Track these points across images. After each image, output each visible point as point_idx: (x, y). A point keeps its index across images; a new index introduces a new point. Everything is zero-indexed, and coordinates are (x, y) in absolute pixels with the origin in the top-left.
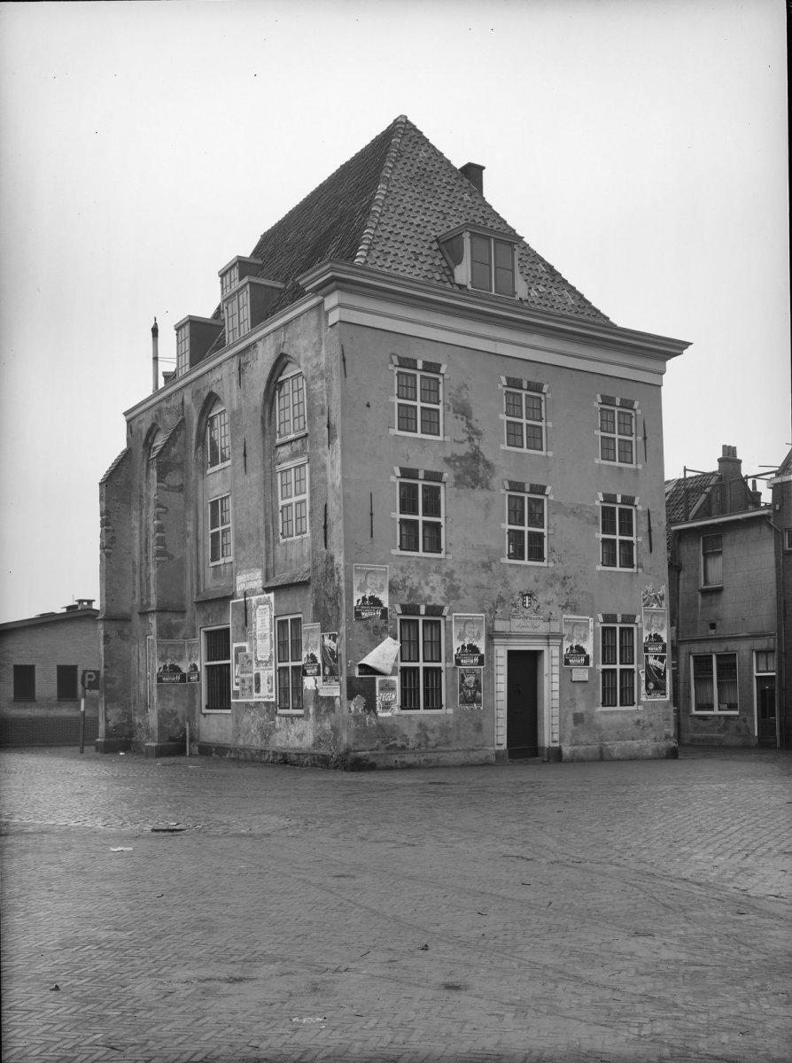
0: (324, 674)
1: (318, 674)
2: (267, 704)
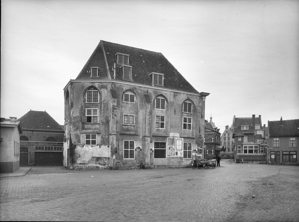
0: (198, 153)
1: (196, 153)
2: (180, 158)
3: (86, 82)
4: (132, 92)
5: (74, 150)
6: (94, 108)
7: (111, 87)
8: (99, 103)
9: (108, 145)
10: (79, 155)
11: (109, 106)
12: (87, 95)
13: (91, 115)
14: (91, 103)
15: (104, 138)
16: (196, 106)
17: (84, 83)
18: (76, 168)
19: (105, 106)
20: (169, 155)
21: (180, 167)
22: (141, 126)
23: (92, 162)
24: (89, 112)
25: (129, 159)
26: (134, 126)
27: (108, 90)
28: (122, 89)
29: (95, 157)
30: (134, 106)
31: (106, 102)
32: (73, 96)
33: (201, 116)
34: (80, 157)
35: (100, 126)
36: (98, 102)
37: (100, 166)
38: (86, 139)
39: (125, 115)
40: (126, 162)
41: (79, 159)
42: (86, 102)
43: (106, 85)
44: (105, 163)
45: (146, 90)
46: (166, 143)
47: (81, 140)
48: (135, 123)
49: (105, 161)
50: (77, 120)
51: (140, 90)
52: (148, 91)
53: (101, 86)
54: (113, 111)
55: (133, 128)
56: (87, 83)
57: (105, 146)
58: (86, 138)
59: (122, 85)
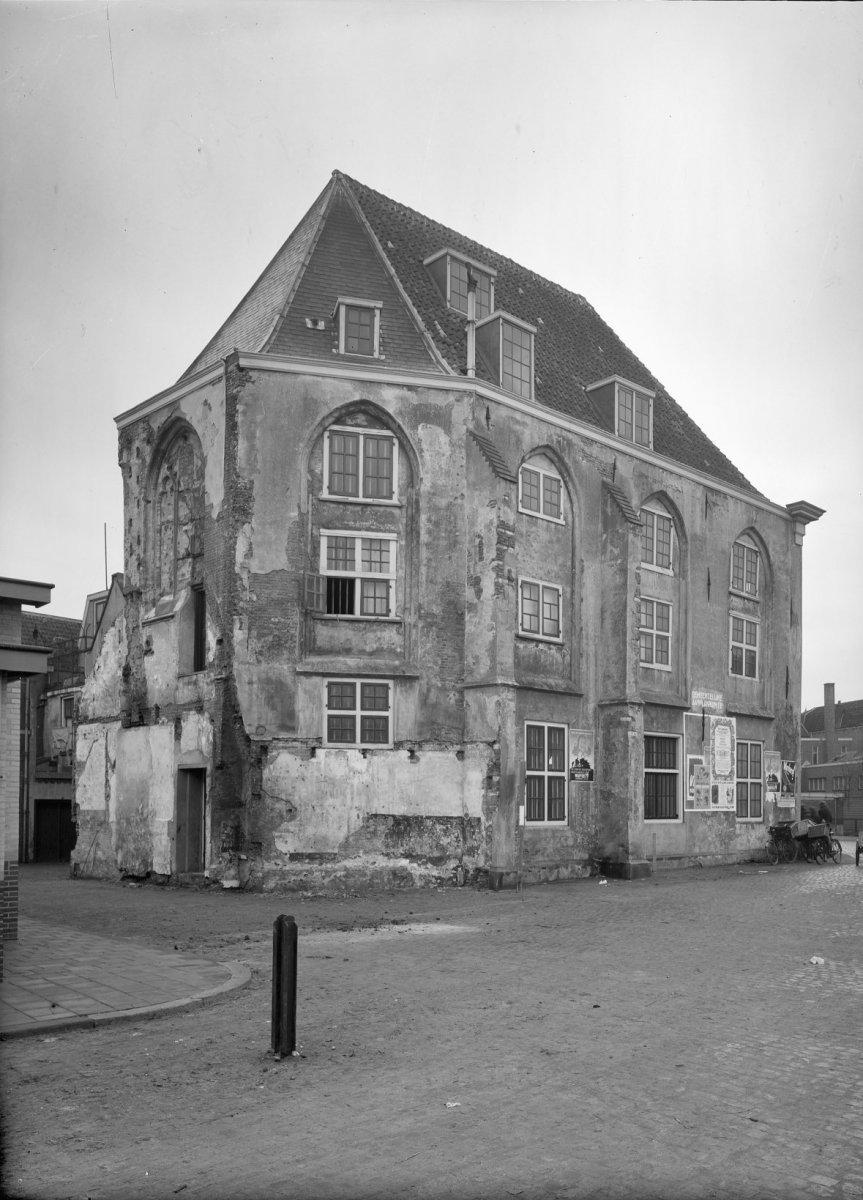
1: (778, 791)
2: (726, 813)
3: (330, 377)
4: (552, 461)
5: (249, 775)
6: (368, 529)
7: (474, 418)
8: (400, 507)
9: (458, 748)
10: (288, 802)
11: (459, 522)
12: (332, 453)
13: (353, 569)
14: (351, 499)
15: (435, 706)
16: (775, 567)
17: (317, 383)
18: (271, 884)
19: (437, 524)
20: (691, 804)
21: (730, 861)
22: (591, 649)
23: (368, 845)
24: (342, 551)
25: (546, 823)
26: (560, 646)
27: (455, 437)
28: (519, 441)
29: (385, 817)
30: (558, 540)
31: (443, 502)
32: (252, 448)
33: (792, 613)
34: (293, 818)
35: (406, 636)
36: (390, 498)
37: (417, 869)
38: (327, 712)
39: (523, 582)
40: (535, 843)
41: (288, 831)
42: (325, 494)
43: (443, 405)
44: (443, 849)
45: (609, 459)
46: (675, 740)
47: (301, 716)
48: (566, 632)
49: (445, 841)
50: (275, 595)
51: (587, 456)
52: (615, 465)
53: (417, 408)
54: (500, 556)
55: (558, 656)
56: (336, 382)
57: (440, 754)
58: (330, 707)
59: (518, 416)
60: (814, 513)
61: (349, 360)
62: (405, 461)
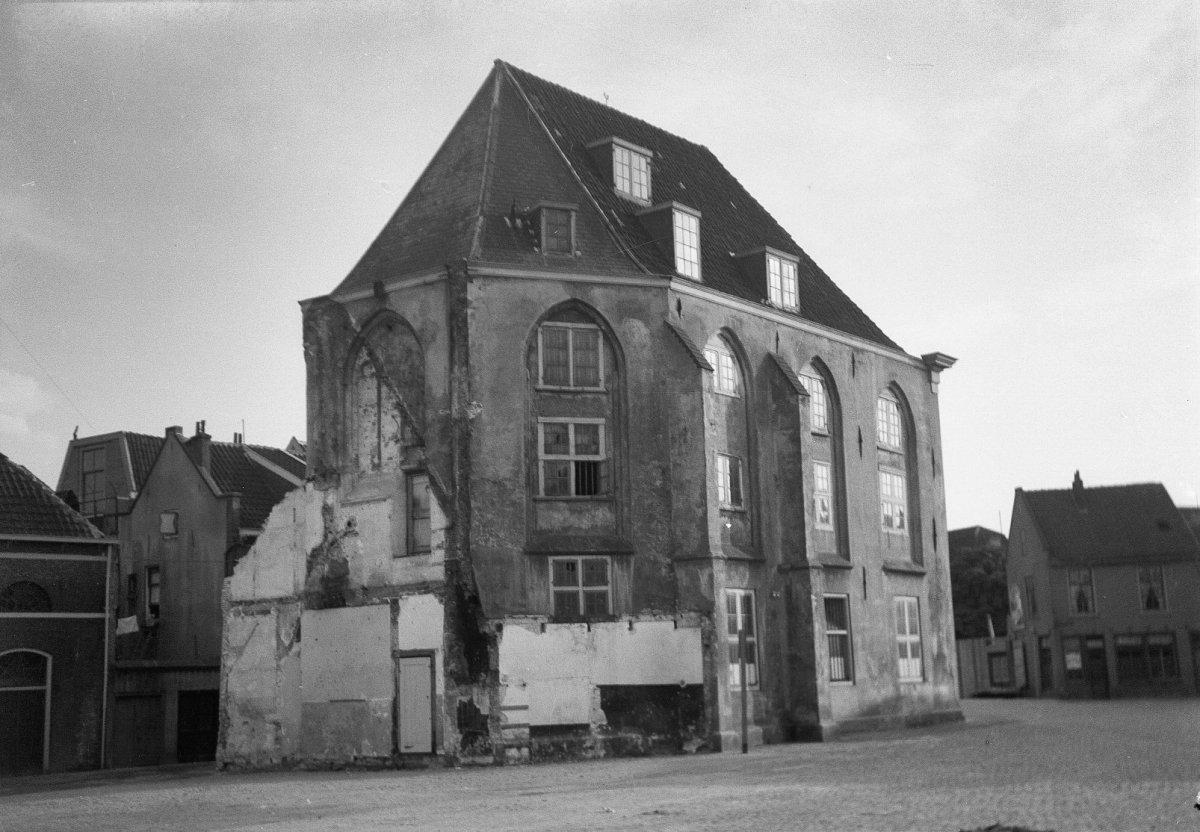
38: (608, 588)
42: (541, 385)
60: (947, 362)
61: (555, 264)
62: (607, 350)
